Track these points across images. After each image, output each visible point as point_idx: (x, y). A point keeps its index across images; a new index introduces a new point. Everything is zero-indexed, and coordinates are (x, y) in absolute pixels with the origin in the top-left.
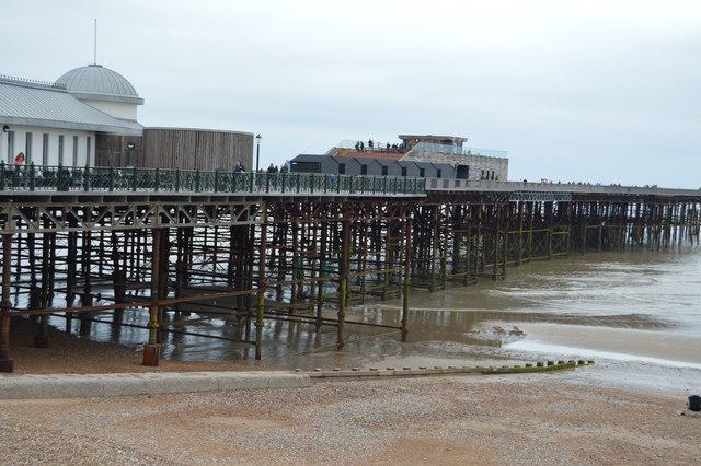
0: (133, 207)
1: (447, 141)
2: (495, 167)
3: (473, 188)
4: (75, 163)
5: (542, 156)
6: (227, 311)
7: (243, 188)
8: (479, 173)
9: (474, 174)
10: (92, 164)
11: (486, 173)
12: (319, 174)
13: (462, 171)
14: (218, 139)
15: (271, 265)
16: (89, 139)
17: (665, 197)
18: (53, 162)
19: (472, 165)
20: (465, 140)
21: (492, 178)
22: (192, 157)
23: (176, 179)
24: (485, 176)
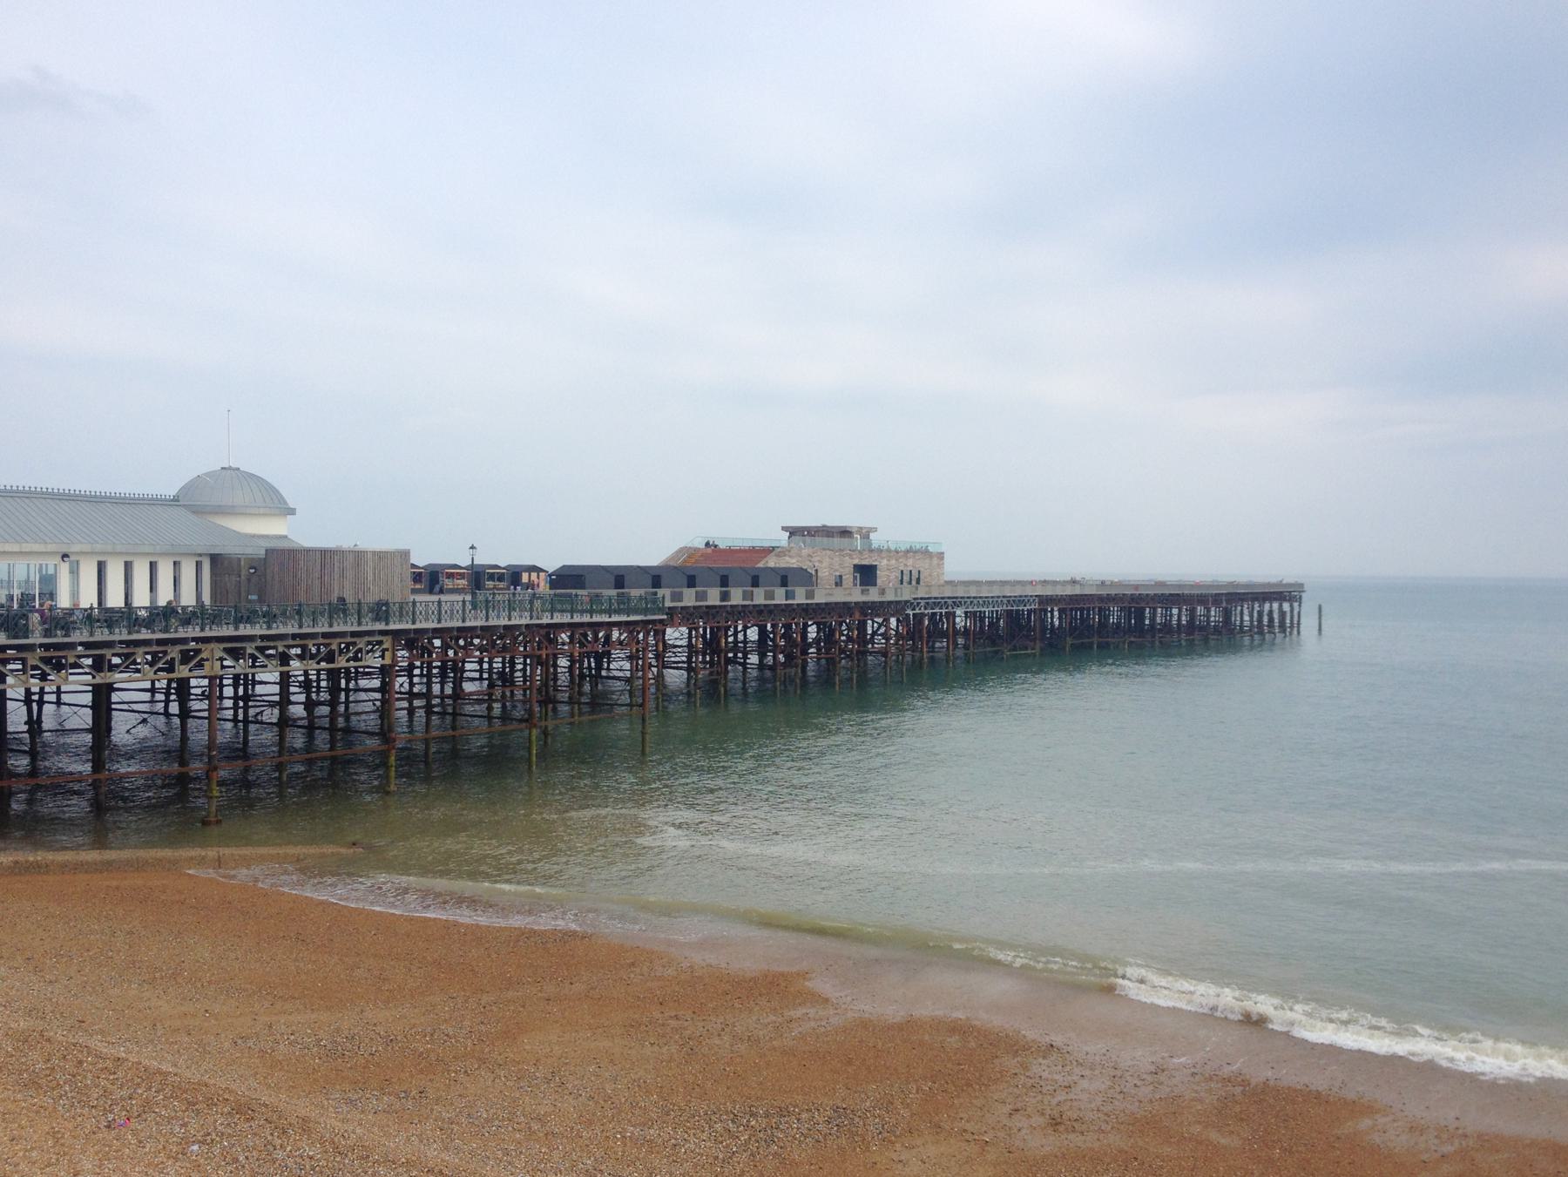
0: (174, 653)
1: (845, 533)
2: (924, 565)
3: (820, 598)
4: (153, 599)
5: (994, 537)
6: (1266, 619)
7: (427, 620)
8: (895, 575)
9: (882, 577)
10: (207, 599)
11: (906, 573)
12: (580, 592)
13: (867, 574)
14: (351, 558)
15: (443, 714)
16: (199, 565)
17: (1191, 596)
18: (141, 599)
19: (882, 564)
20: (875, 530)
21: (918, 581)
22: (317, 582)
23: (339, 608)
24: (906, 578)
